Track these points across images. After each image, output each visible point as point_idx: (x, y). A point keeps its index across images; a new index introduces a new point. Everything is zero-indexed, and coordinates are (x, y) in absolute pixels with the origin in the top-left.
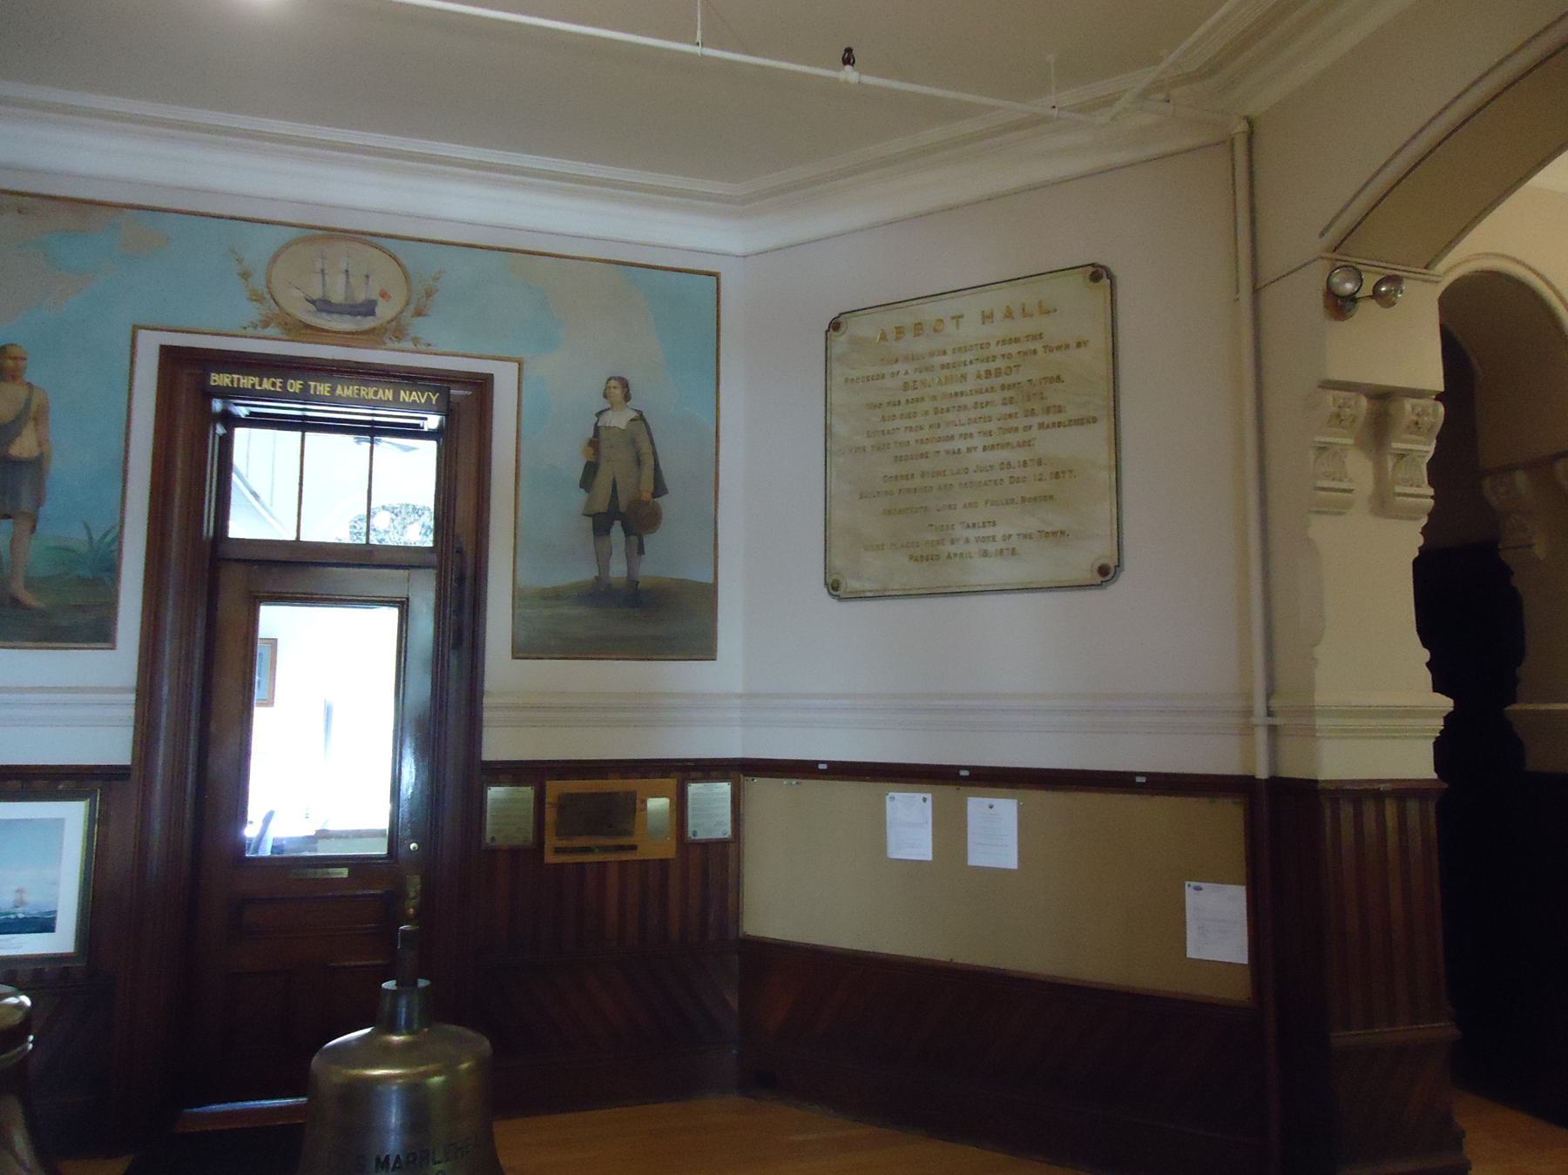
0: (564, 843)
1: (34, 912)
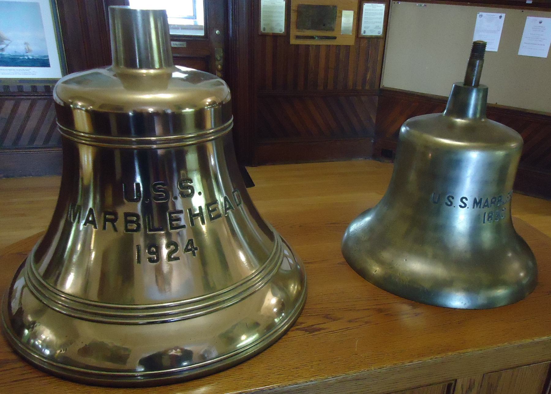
0: (299, 34)
1: (36, 56)
